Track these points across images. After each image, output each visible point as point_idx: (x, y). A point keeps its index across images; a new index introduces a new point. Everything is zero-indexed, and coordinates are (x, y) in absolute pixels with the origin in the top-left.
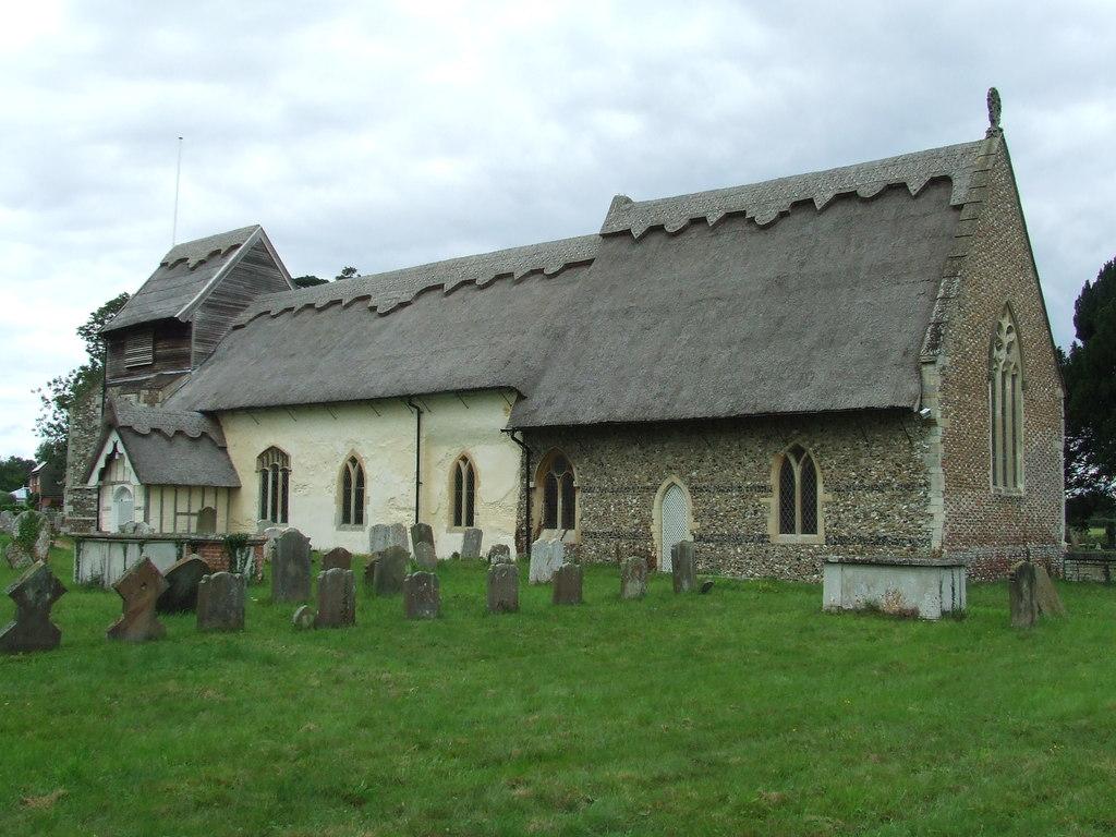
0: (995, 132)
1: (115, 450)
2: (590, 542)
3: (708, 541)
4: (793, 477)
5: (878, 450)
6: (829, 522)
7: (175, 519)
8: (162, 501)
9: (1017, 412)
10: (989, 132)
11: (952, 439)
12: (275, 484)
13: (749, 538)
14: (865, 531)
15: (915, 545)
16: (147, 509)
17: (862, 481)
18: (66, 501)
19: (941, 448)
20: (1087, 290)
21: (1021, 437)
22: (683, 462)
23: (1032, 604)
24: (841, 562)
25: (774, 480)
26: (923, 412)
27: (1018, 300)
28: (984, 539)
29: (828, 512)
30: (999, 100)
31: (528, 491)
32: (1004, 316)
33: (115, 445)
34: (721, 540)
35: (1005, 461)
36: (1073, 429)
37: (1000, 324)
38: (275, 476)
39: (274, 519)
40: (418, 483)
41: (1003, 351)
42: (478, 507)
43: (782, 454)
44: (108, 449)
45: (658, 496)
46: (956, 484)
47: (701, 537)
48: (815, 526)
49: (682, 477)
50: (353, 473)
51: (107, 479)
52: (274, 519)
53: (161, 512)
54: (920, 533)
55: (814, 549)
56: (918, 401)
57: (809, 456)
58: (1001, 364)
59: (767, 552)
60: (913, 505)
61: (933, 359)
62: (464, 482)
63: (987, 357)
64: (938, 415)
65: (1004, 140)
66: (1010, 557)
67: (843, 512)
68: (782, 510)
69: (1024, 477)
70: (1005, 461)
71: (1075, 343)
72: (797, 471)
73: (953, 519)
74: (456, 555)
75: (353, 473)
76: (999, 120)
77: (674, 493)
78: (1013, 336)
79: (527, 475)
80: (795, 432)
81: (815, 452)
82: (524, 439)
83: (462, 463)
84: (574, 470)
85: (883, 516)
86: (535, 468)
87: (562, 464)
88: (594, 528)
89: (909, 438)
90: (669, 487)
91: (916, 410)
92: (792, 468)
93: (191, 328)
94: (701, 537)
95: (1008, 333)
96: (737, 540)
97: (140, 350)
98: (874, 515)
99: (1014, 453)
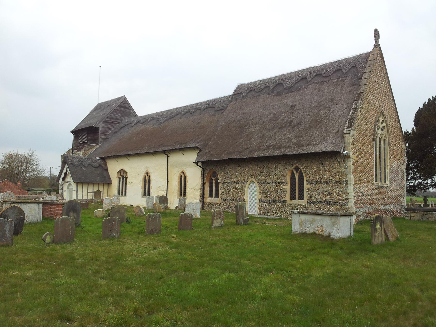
0: (377, 46)
1: (67, 171)
2: (224, 202)
3: (264, 202)
4: (295, 178)
5: (327, 168)
6: (308, 196)
7: (88, 194)
8: (83, 188)
9: (386, 154)
10: (375, 46)
11: (357, 164)
12: (123, 182)
13: (279, 201)
14: (322, 199)
15: (342, 205)
16: (77, 191)
17: (321, 180)
18: (60, 188)
19: (352, 167)
20: (420, 110)
21: (388, 161)
22: (255, 173)
23: (382, 233)
24: (299, 213)
25: (288, 180)
26: (345, 153)
27: (386, 111)
28: (372, 203)
29: (308, 192)
30: (379, 34)
31: (203, 184)
32: (380, 116)
33: (67, 169)
34: (270, 202)
35: (381, 173)
36: (410, 160)
37: (379, 119)
38: (123, 179)
39: (122, 195)
40: (167, 181)
41: (380, 130)
42: (187, 190)
43: (291, 169)
44: (65, 171)
45: (247, 186)
46: (359, 181)
47: (262, 200)
48: (303, 197)
49: (255, 178)
50: (147, 178)
51: (65, 181)
52: (122, 195)
53: (82, 192)
54: (344, 200)
55: (303, 206)
56: (343, 148)
57: (301, 171)
58: (379, 135)
59: (285, 207)
60: (341, 189)
61: (349, 132)
62: (183, 181)
63: (373, 132)
64: (351, 154)
65: (380, 49)
66: (383, 209)
67: (314, 192)
68: (291, 191)
69: (389, 179)
70: (381, 173)
71: (413, 128)
72: (297, 176)
73: (358, 195)
74: (177, 207)
75: (147, 178)
76: (379, 41)
77: (252, 184)
78: (384, 124)
79: (203, 179)
80: (296, 161)
81: (303, 169)
82: (202, 166)
83: (182, 174)
84: (219, 176)
85: (329, 193)
86: (206, 176)
87: (215, 174)
88: (225, 197)
89: (339, 163)
90: (251, 182)
91: (341, 152)
92: (295, 175)
93: (99, 130)
94: (262, 200)
95: (382, 123)
96: (275, 202)
97: (83, 137)
98: (326, 193)
99: (385, 169)
